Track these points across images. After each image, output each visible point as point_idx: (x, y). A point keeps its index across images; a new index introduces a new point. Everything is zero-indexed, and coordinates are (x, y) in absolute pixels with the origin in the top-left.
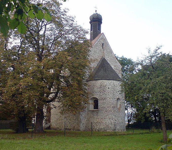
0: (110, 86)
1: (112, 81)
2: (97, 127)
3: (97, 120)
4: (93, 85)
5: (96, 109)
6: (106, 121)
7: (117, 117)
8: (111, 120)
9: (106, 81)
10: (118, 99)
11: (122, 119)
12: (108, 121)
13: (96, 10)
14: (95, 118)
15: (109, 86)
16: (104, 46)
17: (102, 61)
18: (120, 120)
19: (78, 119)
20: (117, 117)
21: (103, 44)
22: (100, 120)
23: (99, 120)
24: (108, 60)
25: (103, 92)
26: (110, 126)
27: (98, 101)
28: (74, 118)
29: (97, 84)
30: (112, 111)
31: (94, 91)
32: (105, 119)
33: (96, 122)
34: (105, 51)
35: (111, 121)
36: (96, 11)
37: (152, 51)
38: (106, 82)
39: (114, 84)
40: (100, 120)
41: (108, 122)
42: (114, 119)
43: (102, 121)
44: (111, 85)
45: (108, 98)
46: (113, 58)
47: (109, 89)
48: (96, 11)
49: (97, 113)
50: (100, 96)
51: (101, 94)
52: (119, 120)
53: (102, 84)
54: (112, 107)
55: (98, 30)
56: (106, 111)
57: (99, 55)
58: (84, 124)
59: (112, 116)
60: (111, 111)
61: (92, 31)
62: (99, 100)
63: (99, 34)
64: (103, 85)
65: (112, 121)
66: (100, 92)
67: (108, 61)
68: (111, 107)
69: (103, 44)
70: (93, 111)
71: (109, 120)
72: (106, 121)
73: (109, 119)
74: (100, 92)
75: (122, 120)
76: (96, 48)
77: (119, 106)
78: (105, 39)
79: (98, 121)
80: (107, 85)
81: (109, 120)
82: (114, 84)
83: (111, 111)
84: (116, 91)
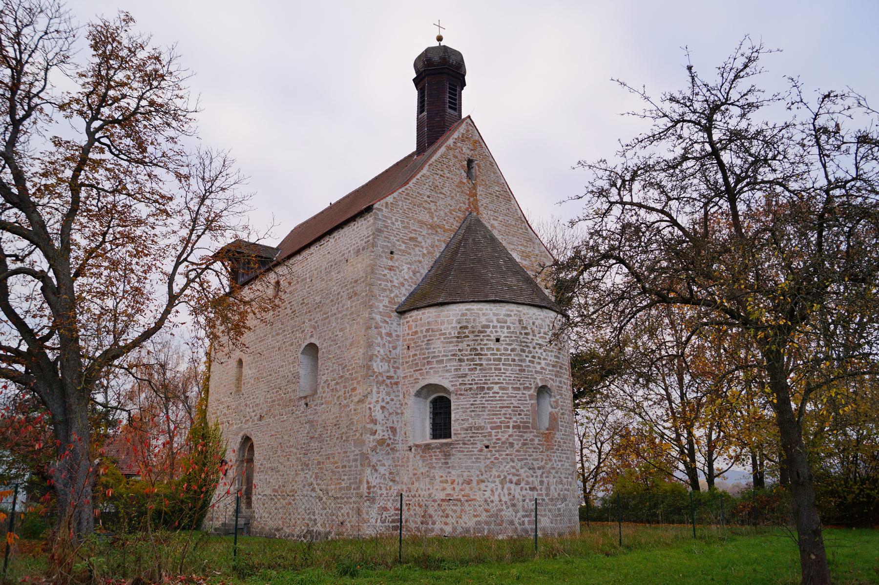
0: (505, 330)
1: (513, 307)
2: (446, 524)
3: (444, 489)
4: (427, 331)
5: (440, 437)
6: (488, 494)
7: (539, 472)
8: (513, 486)
9: (485, 307)
10: (543, 390)
11: (561, 483)
12: (496, 494)
13: (442, 34)
14: (438, 479)
15: (499, 330)
16: (473, 171)
17: (469, 228)
18: (552, 488)
19: (358, 488)
20: (539, 472)
21: (470, 162)
22: (458, 488)
23: (454, 489)
24: (492, 226)
25: (473, 360)
26: (508, 513)
27: (448, 402)
28: (343, 484)
29: (442, 323)
30: (516, 447)
31: (433, 357)
32: (482, 486)
33: (443, 500)
34: (480, 190)
35: (510, 494)
36: (440, 39)
37: (710, 76)
38: (483, 314)
39: (520, 321)
40: (458, 488)
41: (499, 496)
42: (527, 483)
43: (467, 491)
44: (509, 328)
45: (496, 388)
46: (513, 223)
47: (497, 345)
48: (440, 39)
49: (447, 455)
50: (424, 358)
51: (465, 369)
52: (548, 489)
53: (468, 321)
54: (514, 427)
55: (450, 107)
56: (487, 447)
57: (453, 203)
58: (385, 509)
59: (513, 467)
60: (512, 445)
61: (425, 113)
62: (453, 398)
63: (452, 123)
64: (473, 327)
65: (516, 491)
66: (460, 360)
67: (495, 233)
68: (511, 425)
69: (470, 162)
70: (428, 447)
71: (503, 488)
72: (488, 494)
73: (503, 483)
74: (460, 360)
75: (561, 486)
76: (441, 173)
77: (546, 423)
78: (479, 143)
79: (449, 491)
80: (491, 324)
81: (503, 488)
82: (520, 321)
83: (512, 445)
84: (530, 352)
